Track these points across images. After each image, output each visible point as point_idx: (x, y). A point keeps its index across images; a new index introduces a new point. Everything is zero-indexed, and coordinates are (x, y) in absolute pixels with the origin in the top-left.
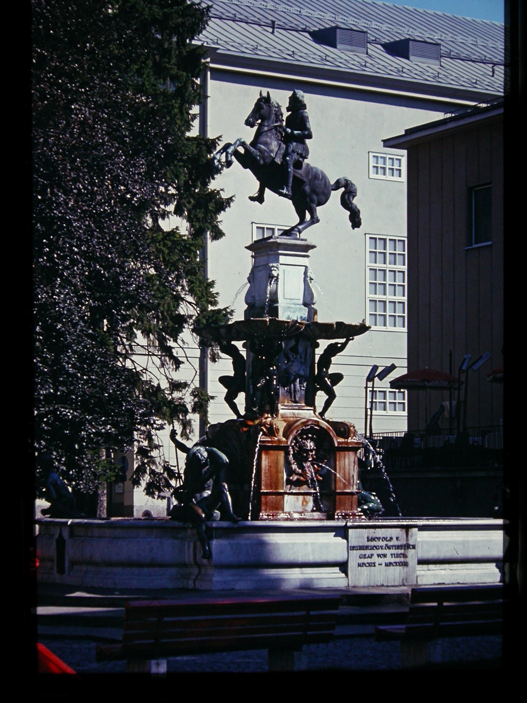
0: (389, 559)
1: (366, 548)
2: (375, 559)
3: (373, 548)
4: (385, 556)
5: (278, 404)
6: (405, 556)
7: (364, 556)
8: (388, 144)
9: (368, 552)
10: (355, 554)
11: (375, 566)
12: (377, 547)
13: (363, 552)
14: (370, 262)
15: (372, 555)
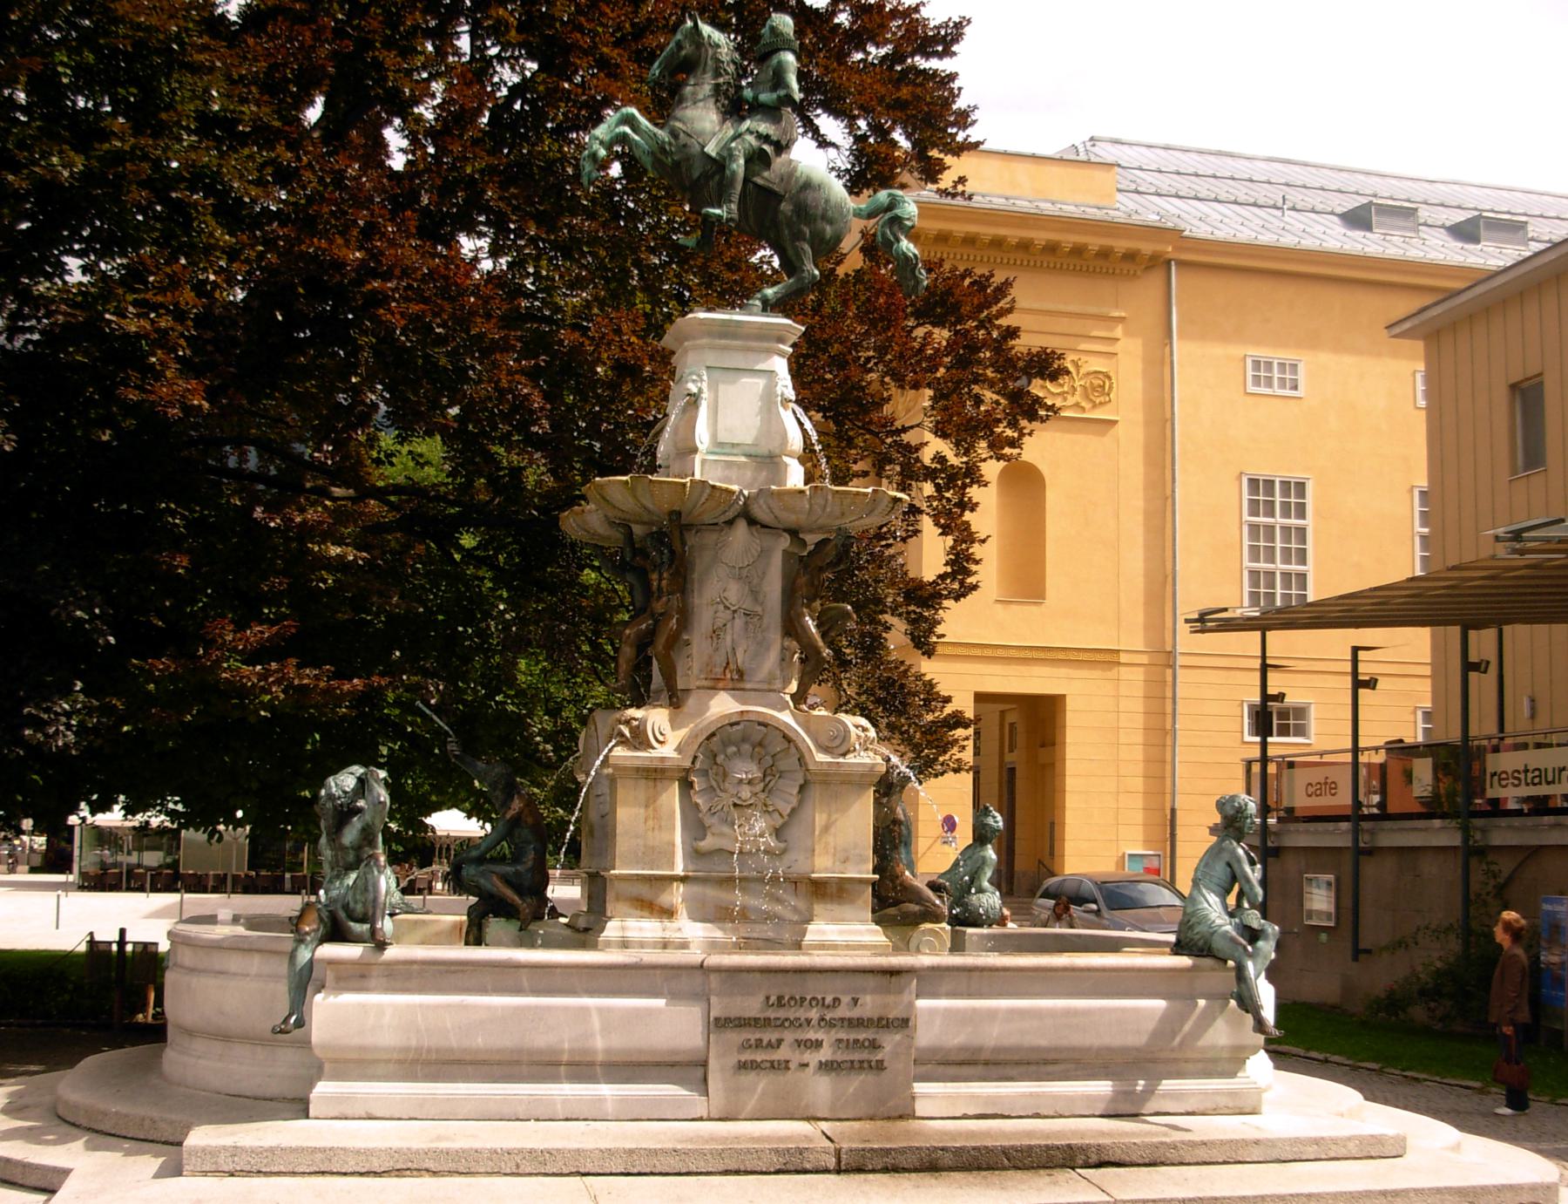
0: (825, 1054)
1: (767, 1023)
2: (796, 1057)
3: (781, 1024)
4: (818, 1044)
5: (126, 398)
6: (874, 1045)
7: (759, 1044)
8: (1397, 330)
9: (769, 1036)
10: (735, 1037)
11: (788, 1068)
12: (796, 1024)
13: (753, 1035)
14: (1250, 561)
15: (780, 1042)
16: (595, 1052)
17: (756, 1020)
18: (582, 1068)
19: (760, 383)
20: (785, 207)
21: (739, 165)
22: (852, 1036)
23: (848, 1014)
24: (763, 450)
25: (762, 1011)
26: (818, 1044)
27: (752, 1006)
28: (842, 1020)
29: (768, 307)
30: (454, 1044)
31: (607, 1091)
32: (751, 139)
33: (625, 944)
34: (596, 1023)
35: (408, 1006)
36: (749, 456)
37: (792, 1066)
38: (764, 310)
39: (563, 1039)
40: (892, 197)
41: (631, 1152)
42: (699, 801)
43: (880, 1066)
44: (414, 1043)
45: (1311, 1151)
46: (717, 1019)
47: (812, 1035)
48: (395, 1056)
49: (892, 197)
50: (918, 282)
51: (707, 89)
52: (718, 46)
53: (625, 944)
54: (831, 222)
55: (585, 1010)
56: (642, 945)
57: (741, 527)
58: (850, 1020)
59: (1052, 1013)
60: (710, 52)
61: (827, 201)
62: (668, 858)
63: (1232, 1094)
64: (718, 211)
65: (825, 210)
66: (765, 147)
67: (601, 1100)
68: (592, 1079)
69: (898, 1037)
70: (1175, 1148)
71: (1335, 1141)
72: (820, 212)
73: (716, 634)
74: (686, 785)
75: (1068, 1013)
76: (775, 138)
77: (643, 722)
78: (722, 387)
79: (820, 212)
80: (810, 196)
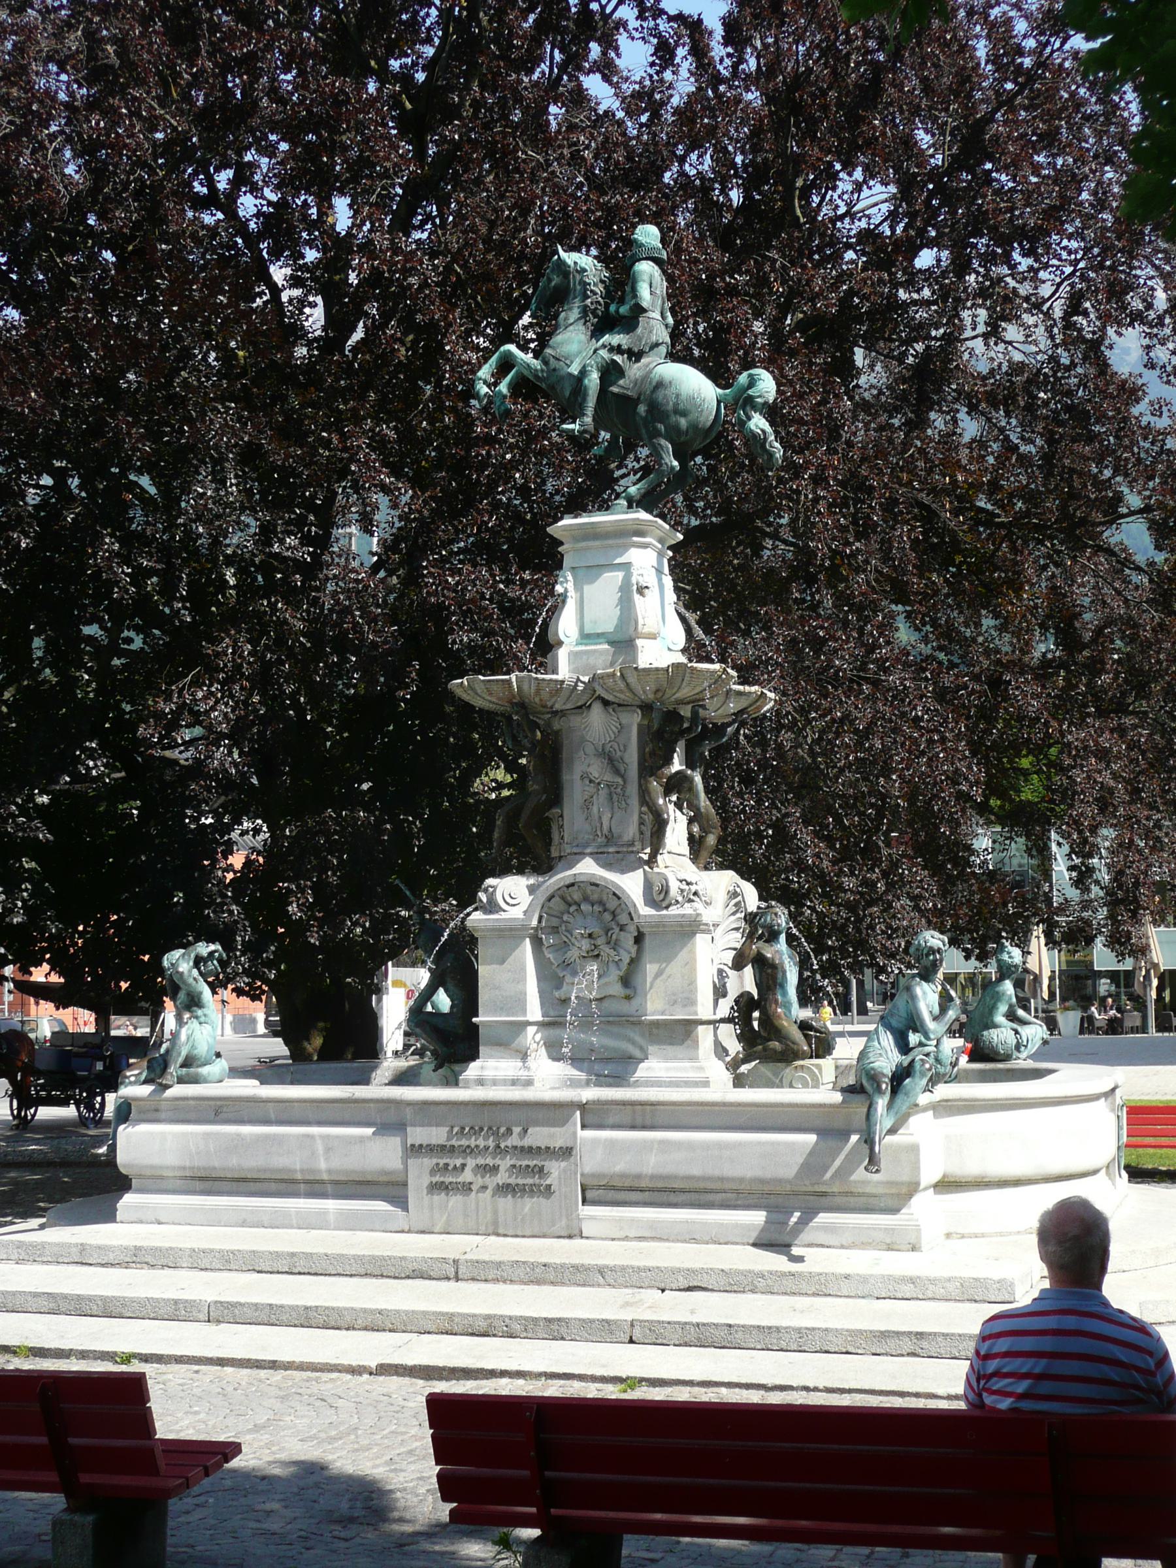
2: (479, 1181)
3: (468, 1151)
4: (494, 1169)
10: (428, 1162)
15: (464, 1166)
16: (319, 1171)
17: (443, 1147)
18: (315, 1187)
19: (620, 575)
20: (642, 409)
21: (593, 379)
22: (525, 1163)
23: (519, 1144)
24: (619, 637)
25: (449, 1139)
26: (494, 1169)
27: (437, 1135)
28: (515, 1148)
29: (631, 503)
30: (217, 1164)
31: (331, 1205)
32: (603, 353)
33: (481, 1082)
34: (320, 1148)
35: (184, 1134)
36: (611, 643)
37: (474, 1187)
38: (630, 506)
39: (292, 1162)
40: (750, 376)
41: (293, 1255)
42: (551, 956)
43: (548, 1191)
44: (188, 1164)
45: (908, 1290)
46: (413, 1146)
47: (489, 1161)
48: (178, 1174)
49: (750, 376)
50: (771, 455)
51: (575, 314)
52: (584, 270)
53: (481, 1082)
54: (684, 414)
55: (311, 1137)
56: (495, 1082)
57: (597, 709)
58: (522, 1148)
59: (707, 1146)
60: (578, 277)
61: (678, 396)
62: (522, 1007)
63: (889, 1230)
64: (571, 426)
65: (676, 404)
66: (618, 358)
67: (324, 1213)
68: (323, 1195)
69: (563, 1164)
70: (763, 1277)
71: (933, 1281)
72: (670, 406)
73: (587, 804)
74: (537, 943)
75: (720, 1145)
76: (625, 347)
77: (495, 887)
78: (586, 588)
79: (670, 406)
80: (660, 395)
